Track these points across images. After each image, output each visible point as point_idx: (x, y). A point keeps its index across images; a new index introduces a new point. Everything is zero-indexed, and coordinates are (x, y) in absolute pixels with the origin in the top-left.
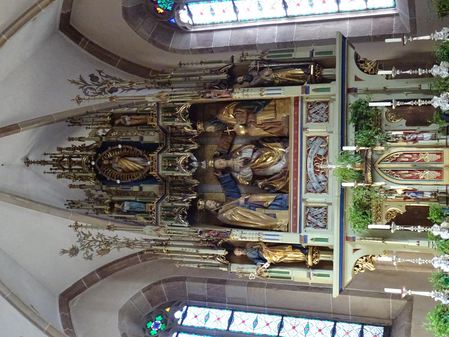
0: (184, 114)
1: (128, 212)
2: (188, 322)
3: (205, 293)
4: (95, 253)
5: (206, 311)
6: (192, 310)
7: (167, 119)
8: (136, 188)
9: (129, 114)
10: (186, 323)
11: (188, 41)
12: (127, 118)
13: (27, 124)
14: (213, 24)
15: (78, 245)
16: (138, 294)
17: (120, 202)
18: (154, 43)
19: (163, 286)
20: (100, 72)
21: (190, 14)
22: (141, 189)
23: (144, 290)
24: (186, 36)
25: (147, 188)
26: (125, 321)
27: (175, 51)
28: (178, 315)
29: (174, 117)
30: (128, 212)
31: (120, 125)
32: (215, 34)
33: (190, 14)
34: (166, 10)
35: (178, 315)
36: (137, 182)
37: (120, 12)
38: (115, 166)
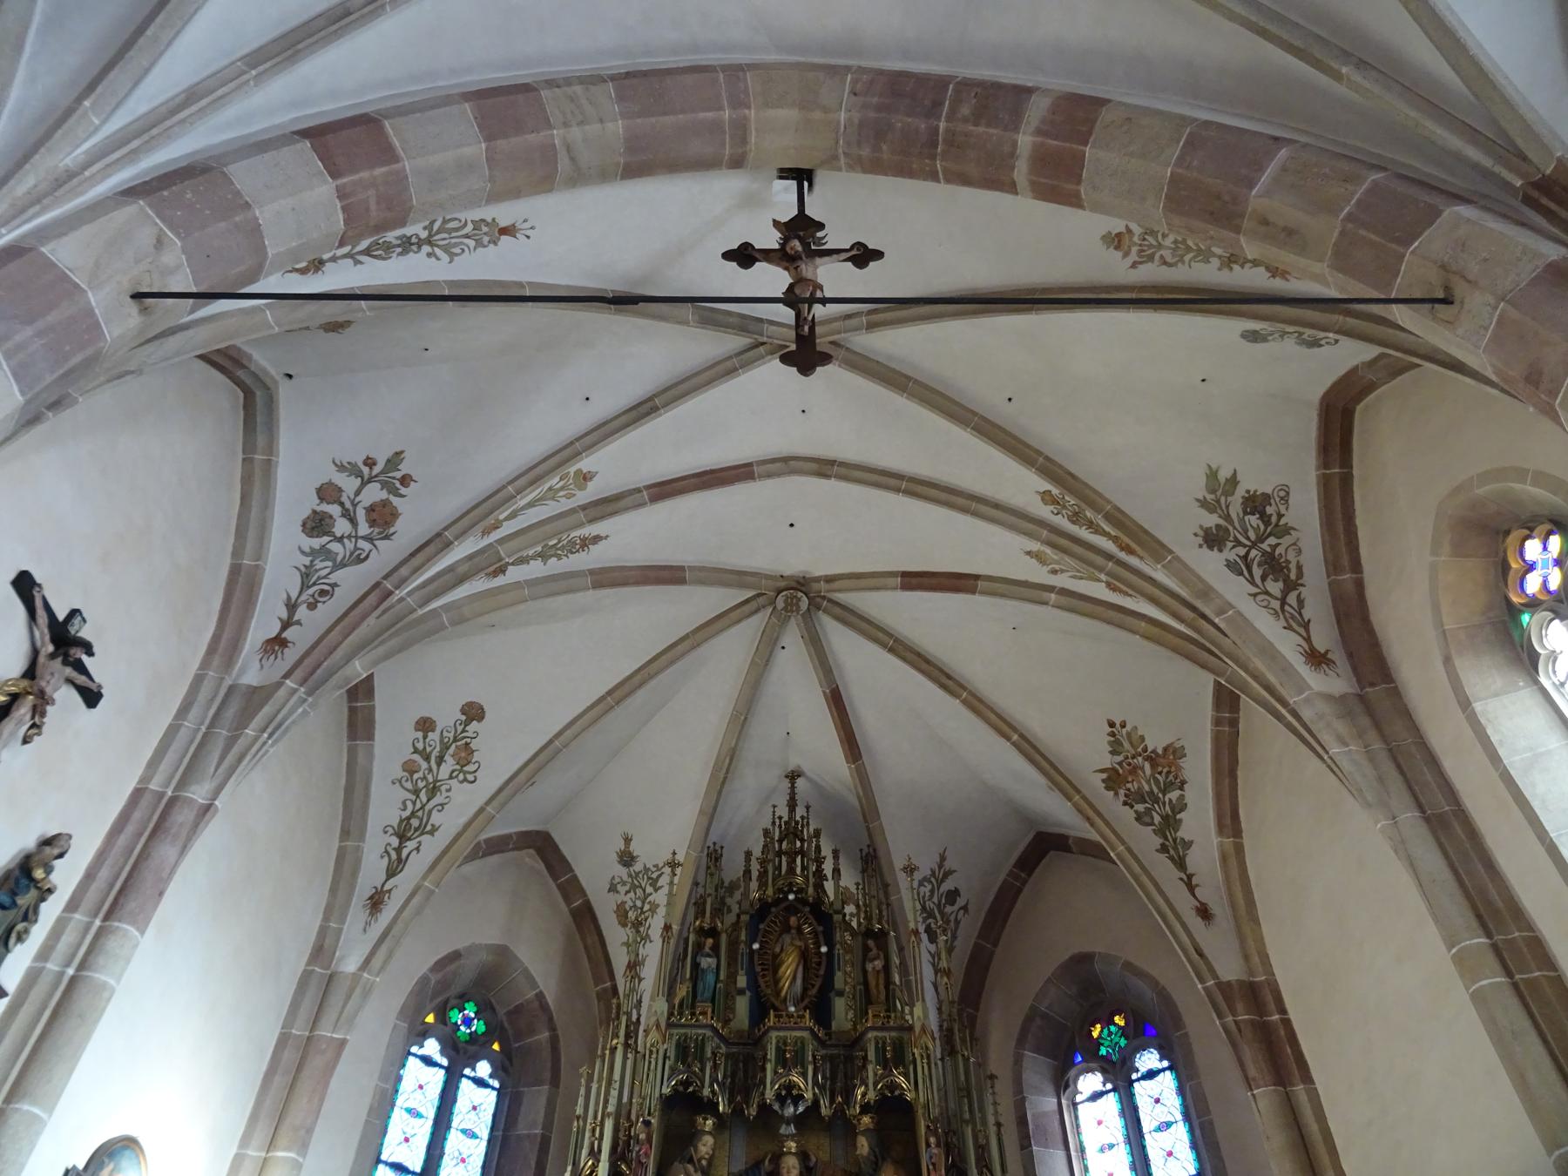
0: (893, 1086)
1: (696, 966)
2: (467, 1091)
3: (522, 1129)
4: (620, 898)
5: (484, 1133)
6: (488, 1099)
7: (881, 1051)
8: (742, 981)
9: (887, 968)
10: (466, 1086)
11: (1041, 1092)
12: (879, 964)
13: (862, 777)
14: (1082, 1150)
15: (638, 867)
16: (534, 984)
17: (716, 949)
18: (1029, 1020)
19: (545, 1035)
20: (965, 908)
21: (1096, 1096)
22: (741, 992)
23: (540, 996)
24: (1050, 1089)
25: (742, 1005)
26: (484, 957)
27: (1018, 1061)
28: (483, 1069)
29: (884, 1062)
30: (696, 966)
31: (866, 949)
32: (1061, 1154)
33: (1096, 1096)
34: (1098, 1043)
35: (483, 1069)
36: (753, 984)
37: (1087, 948)
38: (787, 938)
